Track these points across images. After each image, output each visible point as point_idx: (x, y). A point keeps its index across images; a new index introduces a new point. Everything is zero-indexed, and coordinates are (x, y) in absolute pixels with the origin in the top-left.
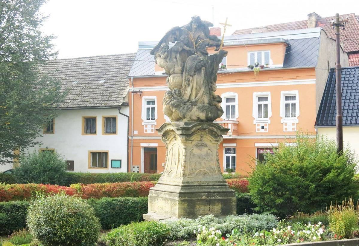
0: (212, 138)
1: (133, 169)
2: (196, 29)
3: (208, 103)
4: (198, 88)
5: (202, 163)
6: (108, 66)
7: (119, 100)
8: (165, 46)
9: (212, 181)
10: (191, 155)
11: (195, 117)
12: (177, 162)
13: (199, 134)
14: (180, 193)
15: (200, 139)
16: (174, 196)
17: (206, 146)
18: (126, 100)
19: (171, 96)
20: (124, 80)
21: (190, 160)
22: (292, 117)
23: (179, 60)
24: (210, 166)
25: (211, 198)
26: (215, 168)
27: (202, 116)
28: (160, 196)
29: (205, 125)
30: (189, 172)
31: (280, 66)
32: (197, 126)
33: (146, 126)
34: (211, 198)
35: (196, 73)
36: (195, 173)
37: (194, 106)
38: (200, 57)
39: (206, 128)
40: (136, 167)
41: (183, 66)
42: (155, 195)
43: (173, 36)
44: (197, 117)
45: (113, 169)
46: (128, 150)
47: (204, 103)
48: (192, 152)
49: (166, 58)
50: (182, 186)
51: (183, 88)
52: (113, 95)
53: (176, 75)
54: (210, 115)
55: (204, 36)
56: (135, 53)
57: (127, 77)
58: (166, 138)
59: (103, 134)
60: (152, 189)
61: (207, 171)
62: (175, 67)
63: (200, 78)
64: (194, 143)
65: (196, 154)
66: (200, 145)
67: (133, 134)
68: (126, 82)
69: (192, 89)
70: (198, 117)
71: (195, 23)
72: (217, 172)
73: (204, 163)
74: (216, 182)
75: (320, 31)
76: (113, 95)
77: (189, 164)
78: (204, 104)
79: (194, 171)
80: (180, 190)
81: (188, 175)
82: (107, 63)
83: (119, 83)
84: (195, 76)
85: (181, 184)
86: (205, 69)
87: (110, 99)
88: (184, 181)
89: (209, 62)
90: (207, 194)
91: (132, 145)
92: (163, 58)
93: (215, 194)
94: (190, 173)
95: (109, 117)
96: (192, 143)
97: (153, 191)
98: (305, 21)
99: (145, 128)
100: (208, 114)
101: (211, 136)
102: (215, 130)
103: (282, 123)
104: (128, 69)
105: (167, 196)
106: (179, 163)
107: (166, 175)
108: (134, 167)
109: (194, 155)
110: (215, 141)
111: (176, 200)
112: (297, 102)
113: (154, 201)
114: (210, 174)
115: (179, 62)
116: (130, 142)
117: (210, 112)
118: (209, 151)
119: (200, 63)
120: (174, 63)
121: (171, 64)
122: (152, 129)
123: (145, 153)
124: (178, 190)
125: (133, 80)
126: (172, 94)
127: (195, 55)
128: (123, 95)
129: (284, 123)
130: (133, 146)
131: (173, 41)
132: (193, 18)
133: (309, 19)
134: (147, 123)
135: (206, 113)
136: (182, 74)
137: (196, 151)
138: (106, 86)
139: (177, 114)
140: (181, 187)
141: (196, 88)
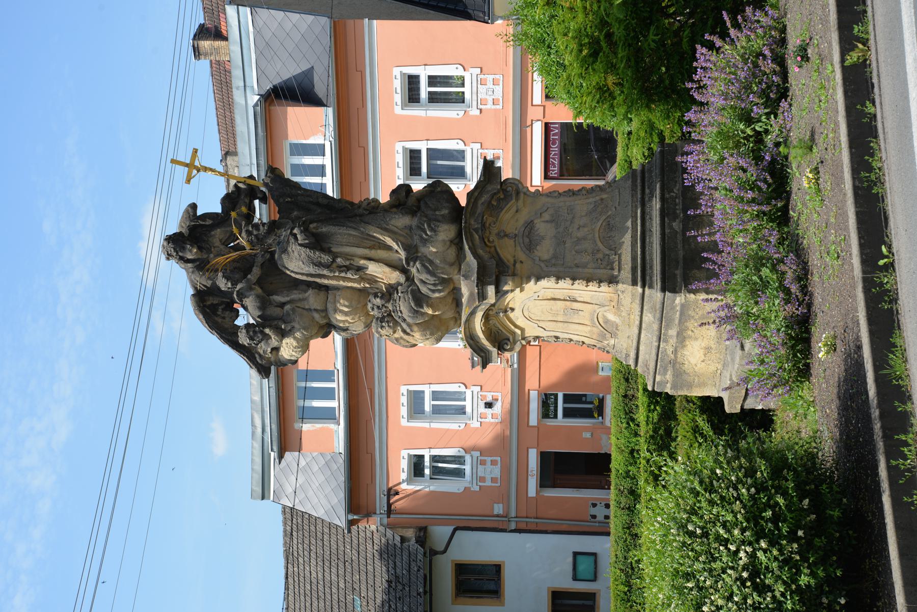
0: (509, 209)
1: (598, 519)
2: (200, 248)
3: (413, 216)
4: (370, 243)
5: (580, 234)
6: (314, 587)
7: (410, 554)
8: (248, 332)
9: (630, 207)
10: (554, 265)
11: (450, 251)
12: (576, 305)
13: (496, 240)
14: (664, 290)
15: (512, 242)
16: (673, 308)
17: (530, 225)
18: (410, 533)
19: (389, 319)
20: (355, 541)
21: (570, 267)
22: (463, 85)
23: (287, 296)
24: (586, 215)
25: (677, 207)
26: (594, 200)
27: (446, 232)
28: (673, 356)
29: (472, 222)
30: (605, 268)
31: (325, 116)
32: (473, 244)
33: (482, 479)
34: (677, 207)
35: (325, 245)
36: (607, 252)
37: (419, 255)
38: (282, 237)
39: (480, 221)
40: (593, 511)
41: (304, 287)
42: (669, 372)
43: (219, 313)
44: (450, 246)
45: (598, 575)
46: (546, 532)
47: (410, 228)
48: (546, 261)
49: (283, 334)
50: (643, 286)
51: (367, 285)
52: (396, 573)
53: (330, 306)
54: (445, 212)
55: (223, 229)
56: (284, 512)
57: (346, 531)
58: (506, 341)
59: (503, 605)
60: (652, 384)
61: (601, 222)
62: (307, 307)
63: (339, 236)
64: (521, 256)
65: (552, 251)
66: (528, 240)
67: (503, 517)
68: (362, 534)
69: (370, 259)
70: (448, 243)
71: (183, 249)
72: (604, 196)
73: (579, 228)
74: (632, 196)
75: (236, 7)
76: (396, 573)
77: (580, 270)
78: (413, 227)
79: (600, 256)
80: (653, 291)
81: (610, 271)
82: (308, 593)
83: (362, 554)
84: (334, 250)
85: (639, 289)
86: (314, 225)
87: (405, 581)
88: (630, 280)
89: (295, 213)
90: (666, 219)
91: (533, 520)
92: (281, 341)
93: (667, 196)
94: (608, 265)
95: (456, 585)
96: (521, 262)
97: (658, 378)
98: (211, 67)
99: (488, 483)
100: (441, 215)
101: (502, 209)
102: (485, 198)
103: (481, 112)
104: (326, 530)
105: (673, 332)
106: (579, 299)
107: (612, 342)
108: (594, 517)
109: (555, 256)
110: (517, 199)
111: (683, 301)
112: (424, 73)
113: (685, 377)
114: (610, 213)
115: (295, 295)
116: (523, 526)
117: (435, 211)
118: (546, 217)
119: (299, 236)
120: (297, 309)
121: (297, 319)
122: (489, 463)
123: (554, 486)
124: (655, 295)
125: (355, 514)
126: (383, 317)
127: (275, 251)
128: (396, 542)
129: (480, 106)
130: (537, 518)
131: (233, 314)
132: (168, 254)
133: (206, 55)
134: (475, 476)
135: (439, 221)
136: (327, 288)
137: (545, 250)
138: (371, 594)
139: (441, 302)
140: (646, 289)
141: (369, 248)
